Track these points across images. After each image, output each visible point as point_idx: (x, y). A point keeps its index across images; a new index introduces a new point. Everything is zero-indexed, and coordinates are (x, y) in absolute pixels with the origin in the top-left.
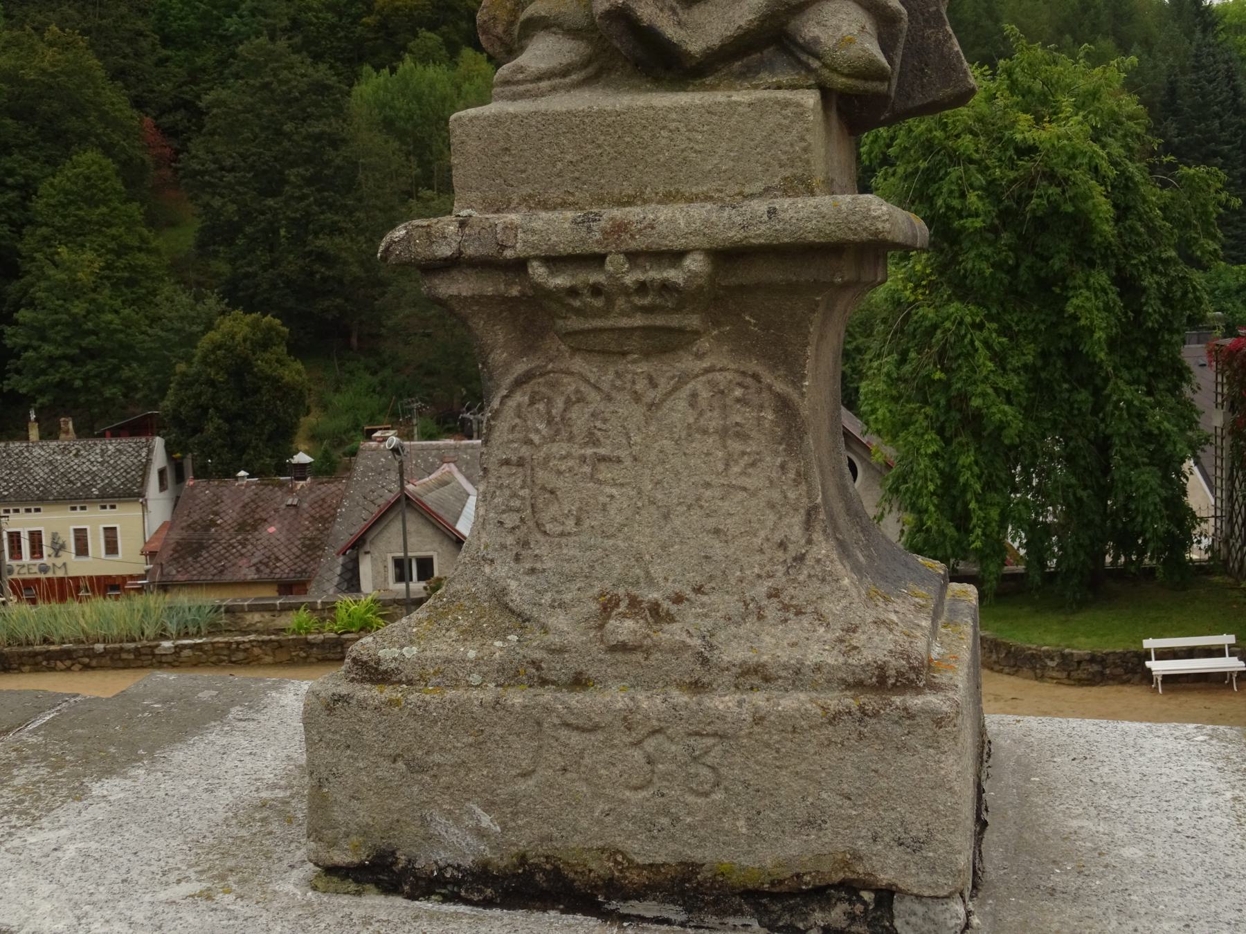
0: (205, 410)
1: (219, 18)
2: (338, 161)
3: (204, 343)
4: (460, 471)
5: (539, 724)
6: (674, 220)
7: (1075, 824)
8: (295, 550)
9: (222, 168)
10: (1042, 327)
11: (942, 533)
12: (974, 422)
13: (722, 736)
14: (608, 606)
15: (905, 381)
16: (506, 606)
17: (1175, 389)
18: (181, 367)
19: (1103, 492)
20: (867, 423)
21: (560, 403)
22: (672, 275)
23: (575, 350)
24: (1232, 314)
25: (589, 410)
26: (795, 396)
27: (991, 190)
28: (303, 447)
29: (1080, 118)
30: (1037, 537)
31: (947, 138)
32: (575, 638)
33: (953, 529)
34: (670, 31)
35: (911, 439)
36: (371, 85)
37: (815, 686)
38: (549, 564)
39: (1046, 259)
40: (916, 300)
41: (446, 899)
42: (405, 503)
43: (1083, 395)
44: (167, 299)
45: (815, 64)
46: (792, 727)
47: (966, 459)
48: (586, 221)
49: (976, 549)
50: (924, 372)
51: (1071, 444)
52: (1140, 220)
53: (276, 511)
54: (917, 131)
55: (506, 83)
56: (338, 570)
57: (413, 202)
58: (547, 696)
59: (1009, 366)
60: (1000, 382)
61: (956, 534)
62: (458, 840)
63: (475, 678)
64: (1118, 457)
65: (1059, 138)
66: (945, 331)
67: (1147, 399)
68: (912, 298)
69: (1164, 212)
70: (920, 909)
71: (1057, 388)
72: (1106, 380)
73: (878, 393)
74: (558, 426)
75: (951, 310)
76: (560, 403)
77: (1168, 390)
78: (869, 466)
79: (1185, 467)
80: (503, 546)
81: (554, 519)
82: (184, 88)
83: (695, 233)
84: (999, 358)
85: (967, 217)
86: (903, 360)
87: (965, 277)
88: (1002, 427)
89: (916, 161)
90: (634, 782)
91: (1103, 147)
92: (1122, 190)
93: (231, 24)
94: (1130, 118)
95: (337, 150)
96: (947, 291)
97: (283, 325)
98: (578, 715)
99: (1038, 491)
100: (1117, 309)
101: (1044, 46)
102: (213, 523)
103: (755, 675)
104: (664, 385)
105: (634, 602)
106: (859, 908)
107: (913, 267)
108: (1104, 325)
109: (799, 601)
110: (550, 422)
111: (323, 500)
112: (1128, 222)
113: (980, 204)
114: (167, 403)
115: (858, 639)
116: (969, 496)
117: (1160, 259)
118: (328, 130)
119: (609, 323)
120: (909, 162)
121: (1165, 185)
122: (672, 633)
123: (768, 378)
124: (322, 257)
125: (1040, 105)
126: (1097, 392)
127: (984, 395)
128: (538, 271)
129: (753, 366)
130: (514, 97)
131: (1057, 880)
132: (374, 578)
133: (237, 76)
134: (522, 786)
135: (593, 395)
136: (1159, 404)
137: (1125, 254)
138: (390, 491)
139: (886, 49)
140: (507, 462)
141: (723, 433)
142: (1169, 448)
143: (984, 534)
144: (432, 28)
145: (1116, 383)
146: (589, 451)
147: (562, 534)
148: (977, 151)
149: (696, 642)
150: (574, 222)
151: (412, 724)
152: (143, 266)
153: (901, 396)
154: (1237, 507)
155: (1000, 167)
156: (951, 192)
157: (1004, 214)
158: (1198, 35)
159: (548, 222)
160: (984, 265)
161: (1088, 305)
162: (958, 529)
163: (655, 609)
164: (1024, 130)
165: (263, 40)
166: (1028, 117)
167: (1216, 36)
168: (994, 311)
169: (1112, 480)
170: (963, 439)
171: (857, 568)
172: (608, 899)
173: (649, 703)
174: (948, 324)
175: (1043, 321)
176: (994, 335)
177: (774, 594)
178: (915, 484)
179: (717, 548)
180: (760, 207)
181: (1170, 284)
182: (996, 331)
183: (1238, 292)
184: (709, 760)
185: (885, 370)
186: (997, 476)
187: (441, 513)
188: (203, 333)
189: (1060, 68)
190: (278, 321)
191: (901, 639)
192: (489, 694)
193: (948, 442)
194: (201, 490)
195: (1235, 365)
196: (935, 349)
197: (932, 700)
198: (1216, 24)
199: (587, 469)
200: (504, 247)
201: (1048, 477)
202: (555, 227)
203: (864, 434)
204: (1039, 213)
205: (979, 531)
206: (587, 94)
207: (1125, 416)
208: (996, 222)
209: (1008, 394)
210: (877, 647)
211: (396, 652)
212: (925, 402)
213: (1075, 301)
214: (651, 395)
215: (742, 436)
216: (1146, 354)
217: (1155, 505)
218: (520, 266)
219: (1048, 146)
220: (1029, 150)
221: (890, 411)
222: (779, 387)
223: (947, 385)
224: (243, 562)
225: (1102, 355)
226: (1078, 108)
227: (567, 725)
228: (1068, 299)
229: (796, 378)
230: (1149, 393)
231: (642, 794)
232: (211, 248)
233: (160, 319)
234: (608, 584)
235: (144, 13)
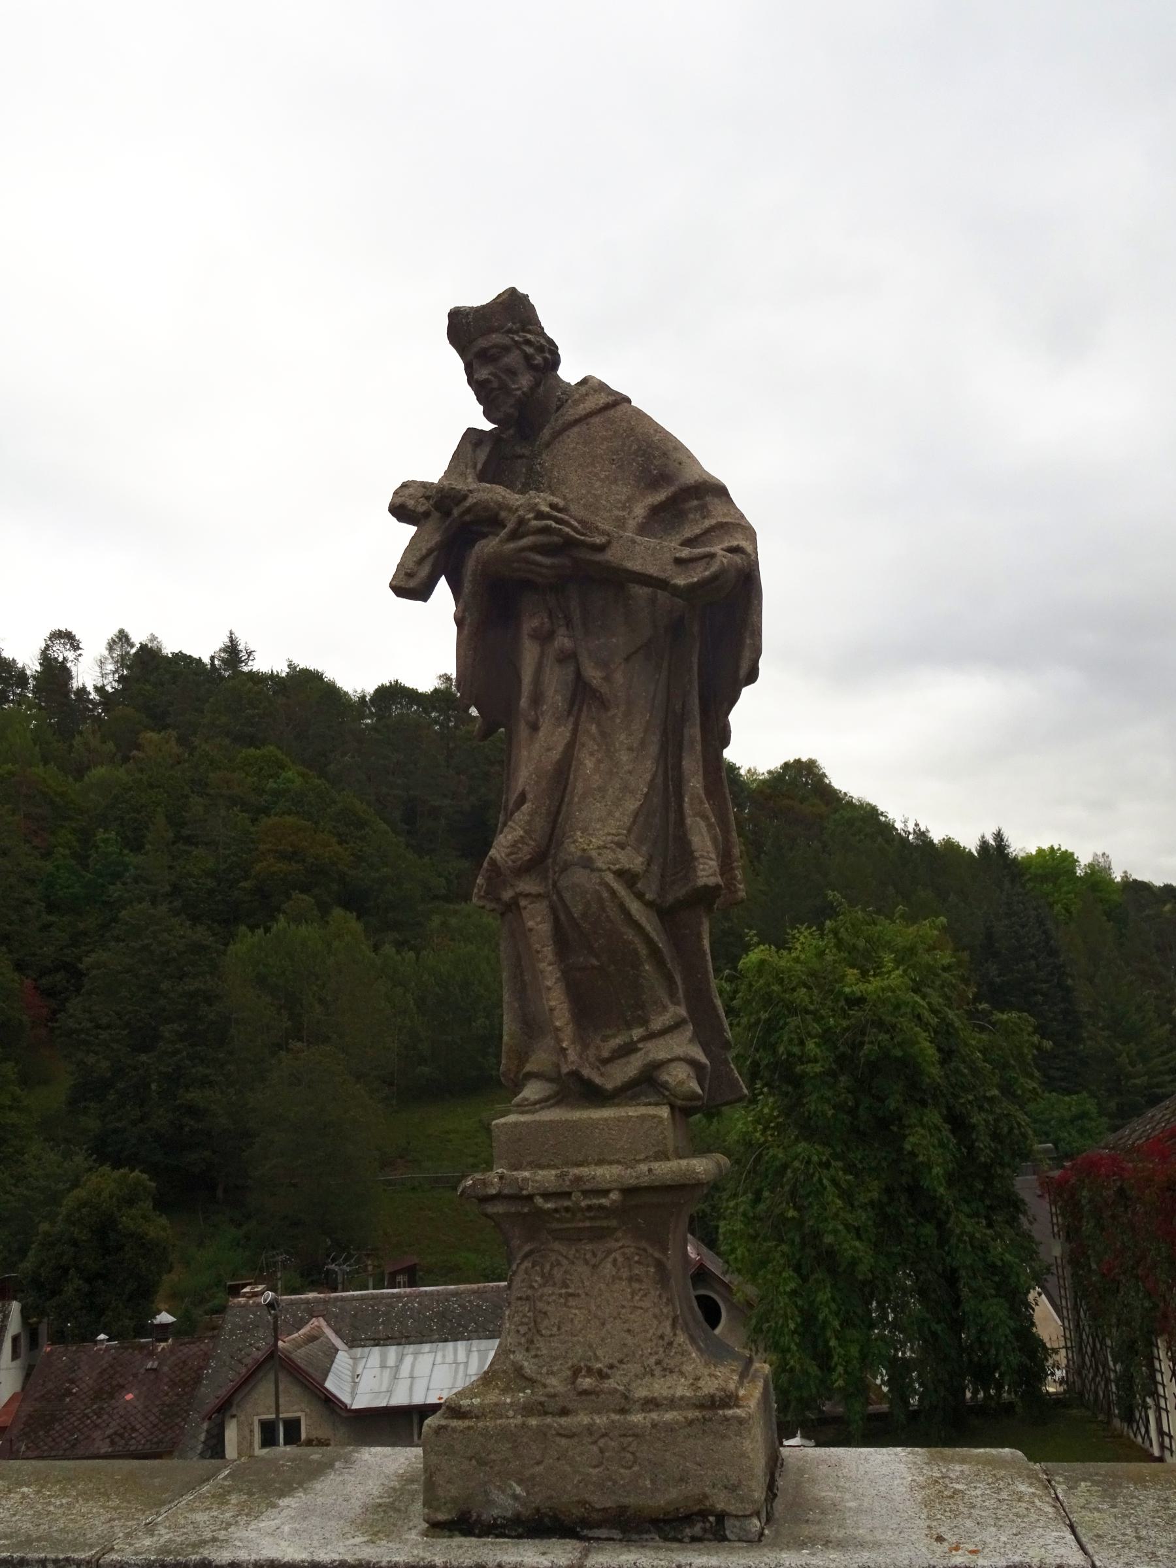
0: (66, 1270)
1: (103, 886)
2: (212, 1017)
3: (69, 1201)
4: (329, 1325)
5: (545, 1435)
6: (605, 1173)
7: (824, 1494)
8: (152, 1418)
9: (98, 1027)
10: (885, 1164)
11: (805, 1372)
12: (828, 1259)
13: (635, 1436)
14: (576, 1372)
15: (761, 1220)
16: (523, 1376)
17: (1012, 1221)
18: (45, 1227)
19: (957, 1325)
20: (727, 1262)
21: (548, 1267)
22: (603, 1201)
23: (555, 1239)
24: (1069, 1143)
25: (563, 1269)
26: (665, 1260)
27: (827, 1037)
28: (162, 1306)
29: (900, 972)
30: (899, 1371)
31: (785, 991)
32: (561, 1389)
33: (815, 1368)
34: (598, 1080)
35: (769, 1277)
36: (246, 941)
37: (680, 1408)
38: (545, 1352)
39: (881, 1100)
40: (766, 1141)
41: (497, 1536)
42: (275, 1362)
43: (928, 1230)
44: (34, 1157)
45: (667, 1093)
46: (670, 1428)
47: (824, 1296)
48: (561, 1176)
49: (839, 1388)
50: (777, 1211)
51: (922, 1278)
52: (964, 1062)
53: (135, 1376)
54: (756, 986)
55: (518, 1105)
56: (202, 1437)
57: (283, 1053)
58: (549, 1420)
59: (856, 1203)
60: (850, 1217)
61: (819, 1373)
62: (505, 1500)
63: (511, 1413)
64: (966, 1289)
65: (883, 990)
66: (795, 1171)
67: (988, 1232)
68: (762, 1140)
69: (984, 1055)
70: (737, 1524)
71: (902, 1221)
72: (948, 1213)
73: (735, 1232)
74: (548, 1279)
75: (799, 1150)
76: (548, 1267)
77: (1007, 1222)
78: (732, 1307)
79: (1031, 1296)
80: (520, 1344)
81: (547, 1328)
82: (65, 951)
83: (615, 1181)
84: (847, 1196)
85: (807, 1063)
86: (758, 1199)
87: (809, 1118)
88: (854, 1263)
89: (758, 1012)
90: (594, 1463)
91: (924, 997)
92: (944, 1035)
93: (115, 891)
94: (946, 969)
95: (210, 1005)
96: (794, 1133)
97: (150, 1180)
98: (565, 1429)
99: (894, 1326)
100: (951, 1146)
101: (864, 910)
102: (68, 1392)
103: (651, 1404)
104: (600, 1255)
105: (590, 1370)
106: (708, 1525)
107: (761, 1111)
108: (940, 1161)
109: (672, 1365)
110: (543, 1276)
111: (184, 1362)
112: (953, 1064)
113: (818, 1051)
114: (27, 1265)
115: (701, 1383)
116: (829, 1333)
117: (985, 1097)
118: (203, 987)
119: (573, 1225)
120: (751, 1014)
121: (982, 1029)
122: (610, 1384)
123: (650, 1250)
124: (192, 1110)
125: (867, 964)
126: (940, 1225)
127: (835, 1232)
128: (539, 1201)
129: (644, 1244)
130: (522, 1113)
131: (811, 1515)
132: (239, 1444)
133: (118, 939)
134: (539, 1469)
135: (565, 1262)
136: (1000, 1236)
137: (952, 1094)
138: (258, 1349)
139: (702, 1090)
140: (520, 1299)
141: (630, 1279)
142: (1013, 1279)
143: (846, 1371)
144: (305, 889)
145: (957, 1217)
146: (563, 1291)
147: (551, 1336)
148: (812, 1002)
149: (621, 1388)
150: (556, 1175)
151: (480, 1438)
152: (13, 1125)
153: (758, 1235)
154: (1084, 1337)
155: (833, 1016)
156: (791, 1040)
157: (841, 1059)
158: (1007, 885)
159: (544, 1176)
160: (826, 1107)
161: (925, 1142)
162: (821, 1368)
163: (600, 1372)
164: (852, 983)
165: (145, 905)
166: (855, 971)
167: (1023, 886)
168: (838, 1150)
169: (964, 1312)
170: (818, 1275)
171: (699, 1349)
172: (582, 1529)
173: (600, 1420)
174: (796, 1164)
175: (885, 1159)
176: (841, 1173)
177: (658, 1363)
178: (776, 1323)
179: (629, 1340)
180: (644, 1167)
181: (996, 1120)
182: (842, 1170)
183: (1072, 1122)
184: (630, 1449)
185: (741, 1210)
186: (855, 1312)
187: (310, 1370)
188: (69, 1190)
189: (879, 928)
190: (145, 1176)
191: (722, 1383)
192: (519, 1420)
193: (805, 1279)
194: (63, 1355)
195: (1065, 1196)
196: (787, 1188)
197: (738, 1411)
198: (1023, 875)
199: (562, 1300)
200: (522, 1189)
201: (903, 1312)
202: (547, 1177)
203: (725, 1273)
204: (873, 1058)
205: (840, 1369)
206: (558, 1111)
207: (969, 1248)
208: (834, 1066)
209: (857, 1229)
210: (709, 1386)
211: (469, 1401)
212: (781, 1241)
213: (911, 1139)
214: (593, 1261)
215: (640, 1281)
216: (982, 1187)
217: (1006, 1336)
218: (530, 1197)
219: (875, 997)
220: (857, 1001)
221: (749, 1250)
222: (657, 1255)
223: (800, 1223)
224: (97, 1434)
225: (941, 1190)
226: (898, 962)
227: (559, 1435)
228: (905, 1137)
229: (664, 1249)
230: (990, 1225)
231: (597, 1470)
232: (82, 1104)
233: (25, 1178)
234: (575, 1361)
235: (32, 882)
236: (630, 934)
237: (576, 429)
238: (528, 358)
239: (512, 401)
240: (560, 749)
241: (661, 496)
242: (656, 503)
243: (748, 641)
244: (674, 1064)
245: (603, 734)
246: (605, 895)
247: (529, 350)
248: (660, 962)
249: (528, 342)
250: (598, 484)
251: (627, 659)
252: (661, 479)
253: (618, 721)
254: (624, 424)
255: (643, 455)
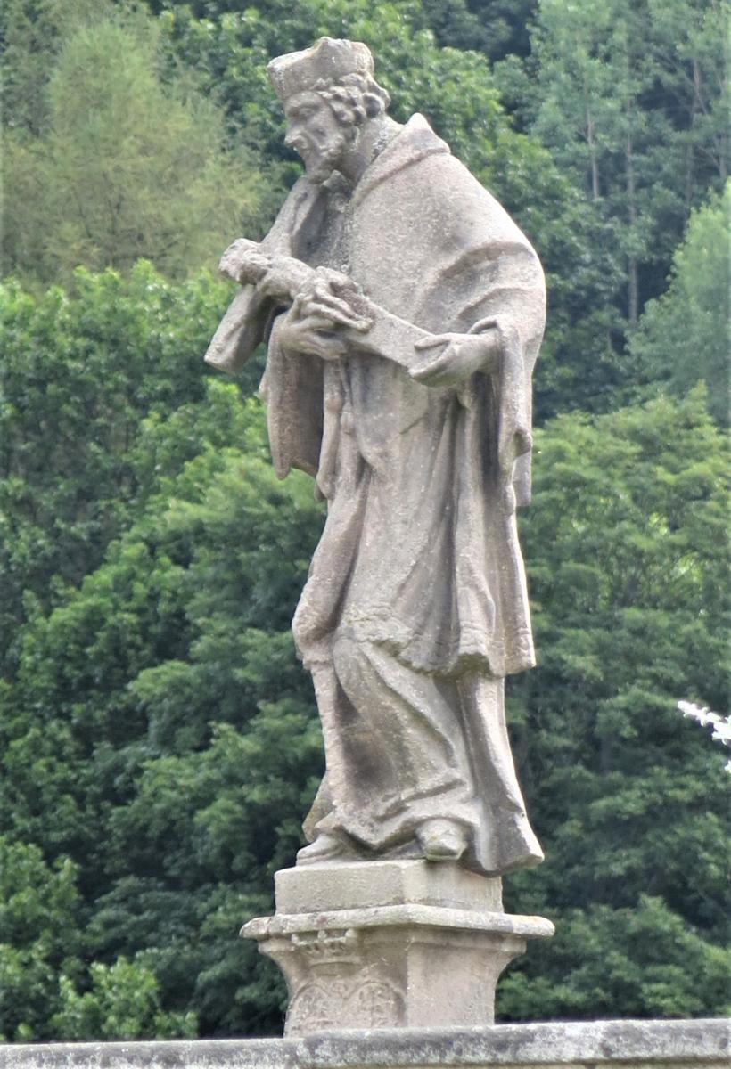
6: (344, 917)
123: (392, 986)
128: (295, 939)
129: (388, 980)
135: (325, 995)
214: (347, 994)
222: (397, 990)
236: (387, 701)
237: (382, 188)
238: (337, 116)
239: (319, 163)
240: (348, 521)
241: (449, 261)
242: (446, 267)
243: (504, 416)
244: (435, 822)
245: (383, 507)
246: (363, 664)
247: (338, 107)
248: (428, 727)
249: (338, 98)
250: (394, 249)
251: (405, 432)
252: (449, 242)
253: (394, 494)
254: (424, 182)
255: (437, 217)
